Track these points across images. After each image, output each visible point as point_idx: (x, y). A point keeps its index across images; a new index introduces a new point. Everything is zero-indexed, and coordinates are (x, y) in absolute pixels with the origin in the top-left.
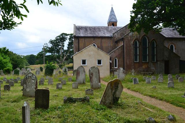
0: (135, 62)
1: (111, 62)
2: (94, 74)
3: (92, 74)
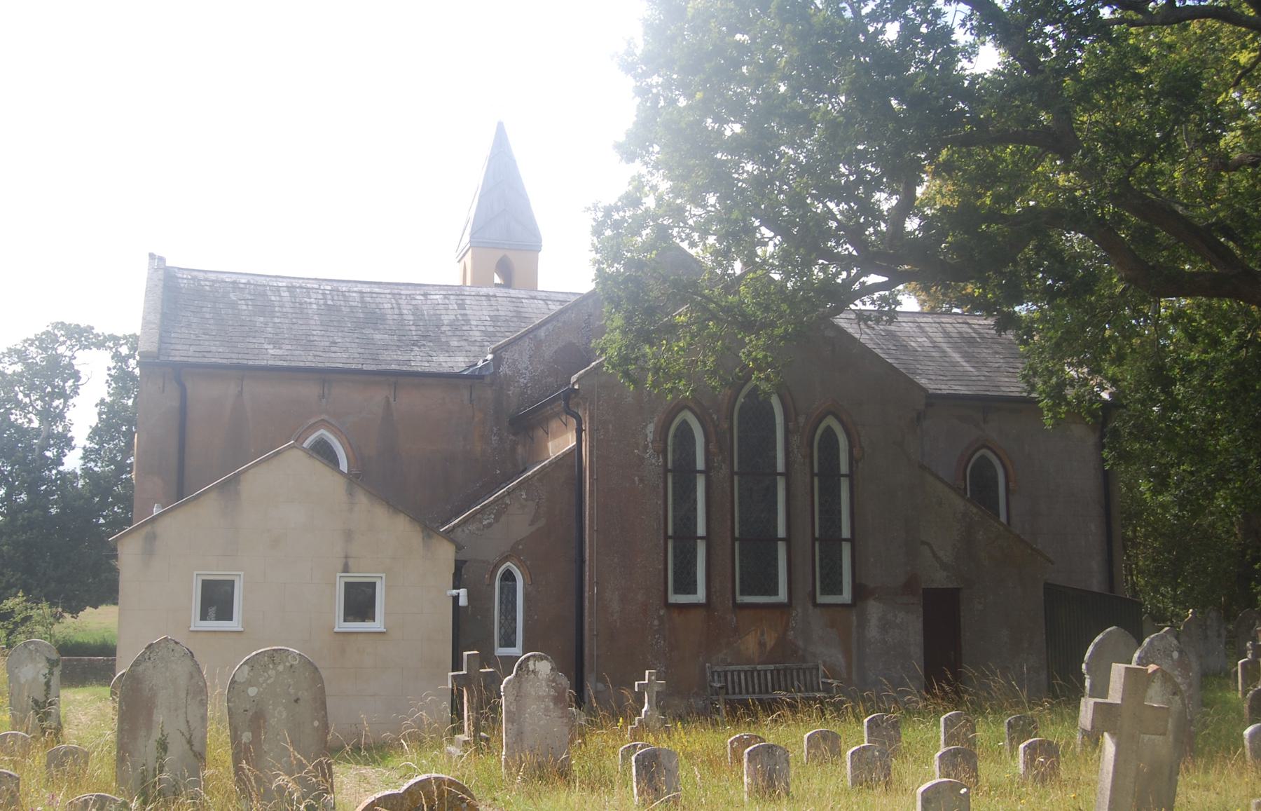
0: (674, 598)
1: (463, 601)
2: (278, 715)
3: (257, 720)
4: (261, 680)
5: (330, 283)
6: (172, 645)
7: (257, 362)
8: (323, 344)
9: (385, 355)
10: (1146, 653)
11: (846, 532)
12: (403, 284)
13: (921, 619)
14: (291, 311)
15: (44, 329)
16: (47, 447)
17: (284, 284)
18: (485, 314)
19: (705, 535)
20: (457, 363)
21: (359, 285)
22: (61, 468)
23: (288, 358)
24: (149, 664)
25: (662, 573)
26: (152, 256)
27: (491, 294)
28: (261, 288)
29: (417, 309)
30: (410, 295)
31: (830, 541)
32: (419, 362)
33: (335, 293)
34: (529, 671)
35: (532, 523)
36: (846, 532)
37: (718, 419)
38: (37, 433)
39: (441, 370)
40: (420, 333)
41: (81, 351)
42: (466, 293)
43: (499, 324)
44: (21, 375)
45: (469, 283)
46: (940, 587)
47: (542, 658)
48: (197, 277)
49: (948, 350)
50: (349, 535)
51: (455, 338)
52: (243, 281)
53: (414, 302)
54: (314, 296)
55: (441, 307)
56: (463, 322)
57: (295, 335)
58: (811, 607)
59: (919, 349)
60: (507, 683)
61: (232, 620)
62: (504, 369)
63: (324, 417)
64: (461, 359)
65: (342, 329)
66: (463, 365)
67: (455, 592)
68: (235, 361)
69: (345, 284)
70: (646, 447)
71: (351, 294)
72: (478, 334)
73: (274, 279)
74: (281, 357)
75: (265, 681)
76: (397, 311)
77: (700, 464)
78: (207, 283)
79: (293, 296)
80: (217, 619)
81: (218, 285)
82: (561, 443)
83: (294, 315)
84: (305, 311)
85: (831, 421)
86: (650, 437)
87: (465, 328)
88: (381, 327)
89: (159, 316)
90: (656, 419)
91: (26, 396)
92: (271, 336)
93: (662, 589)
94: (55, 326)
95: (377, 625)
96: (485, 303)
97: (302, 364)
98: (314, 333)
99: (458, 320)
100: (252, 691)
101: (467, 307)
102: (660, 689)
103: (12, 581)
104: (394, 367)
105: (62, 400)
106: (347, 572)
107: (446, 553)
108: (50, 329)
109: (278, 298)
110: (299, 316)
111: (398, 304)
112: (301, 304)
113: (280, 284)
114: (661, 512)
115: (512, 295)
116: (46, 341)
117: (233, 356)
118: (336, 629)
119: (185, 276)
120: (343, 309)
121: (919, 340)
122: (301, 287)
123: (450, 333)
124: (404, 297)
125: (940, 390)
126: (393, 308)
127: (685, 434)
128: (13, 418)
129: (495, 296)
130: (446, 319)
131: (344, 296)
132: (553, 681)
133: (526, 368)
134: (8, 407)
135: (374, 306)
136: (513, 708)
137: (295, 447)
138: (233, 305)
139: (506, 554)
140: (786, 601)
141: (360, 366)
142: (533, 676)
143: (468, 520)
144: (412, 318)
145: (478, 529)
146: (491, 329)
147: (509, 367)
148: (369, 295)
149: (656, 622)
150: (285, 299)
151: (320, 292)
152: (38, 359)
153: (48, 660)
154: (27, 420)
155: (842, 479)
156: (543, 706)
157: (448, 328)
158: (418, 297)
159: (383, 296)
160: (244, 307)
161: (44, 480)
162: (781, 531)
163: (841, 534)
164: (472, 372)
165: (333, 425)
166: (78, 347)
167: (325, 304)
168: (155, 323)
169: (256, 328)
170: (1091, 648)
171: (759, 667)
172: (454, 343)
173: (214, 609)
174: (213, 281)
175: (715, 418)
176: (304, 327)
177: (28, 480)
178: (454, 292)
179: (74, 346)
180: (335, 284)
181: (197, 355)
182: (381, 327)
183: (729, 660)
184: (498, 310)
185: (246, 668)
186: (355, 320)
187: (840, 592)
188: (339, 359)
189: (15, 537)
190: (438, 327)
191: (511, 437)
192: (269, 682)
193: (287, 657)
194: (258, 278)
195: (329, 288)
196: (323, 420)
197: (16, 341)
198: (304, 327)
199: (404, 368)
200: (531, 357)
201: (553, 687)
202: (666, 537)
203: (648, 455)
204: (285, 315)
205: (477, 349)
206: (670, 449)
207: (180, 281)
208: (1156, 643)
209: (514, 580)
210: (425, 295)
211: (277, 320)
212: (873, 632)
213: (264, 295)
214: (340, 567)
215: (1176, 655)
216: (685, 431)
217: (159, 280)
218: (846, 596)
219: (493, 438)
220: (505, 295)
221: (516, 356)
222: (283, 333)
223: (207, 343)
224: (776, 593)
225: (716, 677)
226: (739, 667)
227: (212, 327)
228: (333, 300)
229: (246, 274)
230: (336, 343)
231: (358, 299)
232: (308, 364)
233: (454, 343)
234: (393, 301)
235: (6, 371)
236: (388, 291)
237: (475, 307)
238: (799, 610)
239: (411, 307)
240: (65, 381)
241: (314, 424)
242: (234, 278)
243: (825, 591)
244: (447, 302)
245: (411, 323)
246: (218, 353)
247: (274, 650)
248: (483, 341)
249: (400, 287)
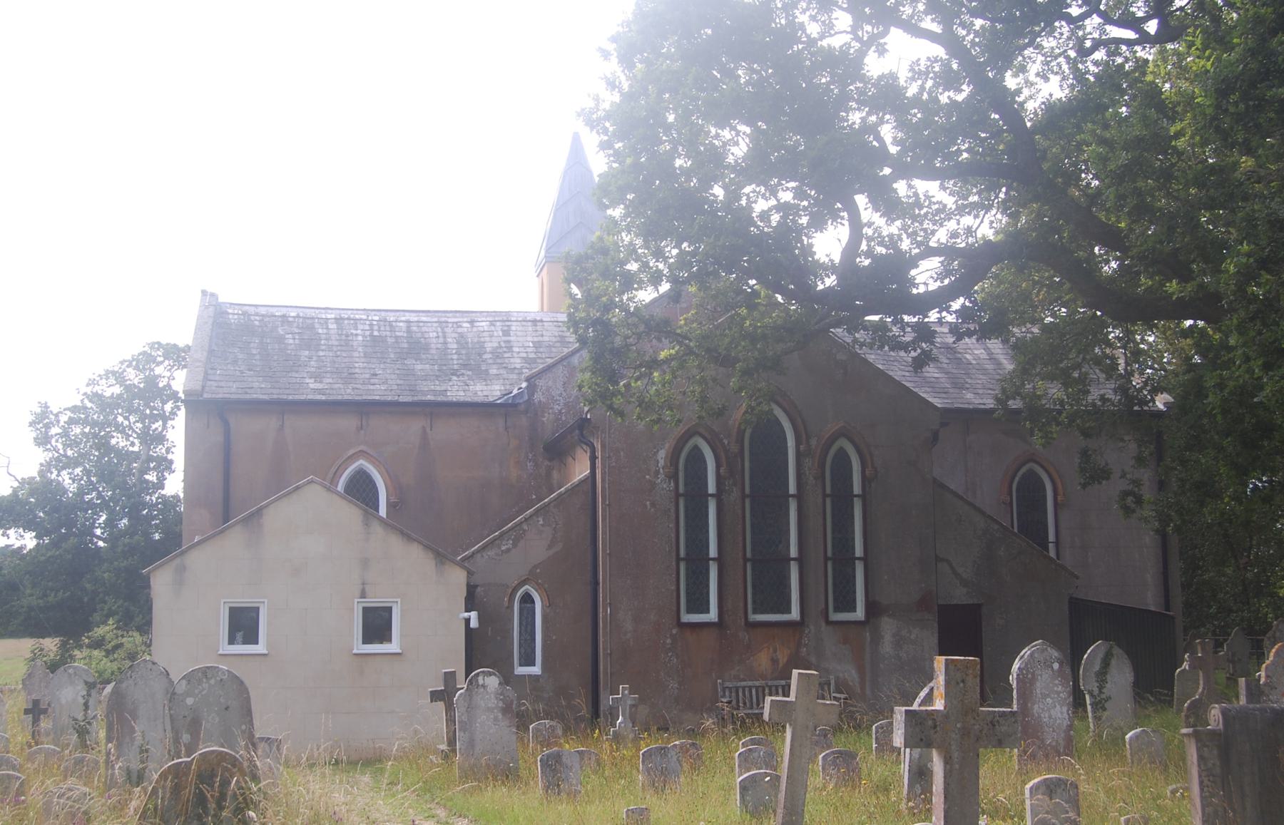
1: (474, 624)
4: (196, 691)
5: (378, 313)
6: (150, 666)
7: (297, 397)
8: (363, 376)
9: (424, 386)
10: (1026, 665)
11: (859, 552)
12: (451, 312)
13: (936, 635)
14: (336, 343)
15: (142, 350)
16: (146, 470)
17: (333, 316)
18: (529, 341)
19: (716, 556)
20: (490, 391)
21: (407, 314)
22: (163, 492)
23: (328, 392)
24: (131, 682)
25: (675, 594)
26: (204, 293)
27: (538, 319)
28: (309, 321)
29: (462, 337)
30: (457, 323)
31: (843, 559)
32: (456, 391)
33: (382, 323)
34: (478, 685)
35: (550, 547)
36: (859, 552)
37: (729, 443)
38: (136, 456)
39: (476, 399)
40: (461, 361)
41: (179, 371)
42: (513, 319)
43: (541, 350)
44: (119, 396)
46: (959, 603)
47: (490, 674)
48: (246, 313)
49: (1005, 362)
50: (365, 563)
51: (495, 366)
52: (293, 314)
53: (460, 330)
54: (361, 327)
55: (485, 334)
56: (505, 349)
57: (337, 369)
58: (823, 624)
59: (974, 362)
60: (459, 697)
61: (257, 643)
62: (538, 397)
63: (362, 447)
64: (497, 387)
65: (385, 360)
66: (498, 393)
67: (466, 615)
68: (275, 397)
69: (393, 314)
70: (657, 472)
71: (398, 324)
72: (518, 361)
73: (323, 311)
74: (320, 391)
75: (200, 692)
76: (441, 340)
78: (257, 318)
79: (340, 328)
80: (245, 643)
81: (267, 319)
82: (580, 470)
83: (339, 348)
84: (351, 343)
86: (662, 463)
87: (506, 355)
88: (424, 356)
89: (205, 354)
90: (667, 445)
91: (127, 418)
92: (313, 370)
93: (675, 609)
94: (152, 346)
95: (393, 647)
96: (530, 329)
97: (340, 397)
98: (357, 365)
99: (501, 347)
100: (190, 701)
101: (512, 333)
102: (633, 702)
103: (113, 608)
104: (430, 397)
105: (160, 423)
106: (365, 598)
107: (458, 578)
108: (146, 349)
109: (325, 331)
110: (343, 348)
111: (444, 333)
112: (347, 336)
113: (329, 316)
114: (673, 535)
115: (559, 320)
117: (275, 391)
118: (355, 651)
119: (236, 312)
120: (389, 339)
121: (976, 352)
122: (349, 319)
123: (490, 361)
124: (450, 325)
125: (984, 404)
126: (438, 337)
127: (696, 459)
128: (113, 441)
129: (542, 321)
130: (489, 346)
131: (391, 326)
132: (501, 694)
133: (560, 395)
134: (107, 430)
135: (419, 335)
136: (464, 718)
137: (312, 481)
138: (281, 339)
139: (523, 578)
140: (799, 618)
141: (396, 398)
142: (482, 690)
143: (487, 546)
144: (455, 346)
145: (497, 555)
146: (532, 356)
147: (543, 394)
148: (415, 324)
149: (669, 641)
150: (332, 332)
151: (368, 322)
152: (136, 382)
153: (86, 683)
154: (129, 443)
156: (492, 716)
157: (490, 356)
158: (465, 325)
159: (429, 324)
160: (291, 341)
161: (144, 505)
163: (854, 553)
164: (506, 400)
165: (372, 456)
166: (176, 367)
167: (371, 335)
168: (200, 361)
169: (300, 363)
171: (770, 683)
172: (493, 371)
173: (241, 633)
174: (263, 315)
175: (726, 443)
176: (346, 360)
177: (129, 505)
178: (500, 319)
179: (173, 367)
180: (383, 314)
181: (240, 391)
182: (424, 356)
183: (742, 677)
184: (542, 336)
185: (184, 682)
186: (398, 350)
187: (707, 611)
188: (378, 391)
189: (116, 563)
190: (480, 355)
191: (547, 463)
192: (203, 693)
193: (217, 672)
194: (308, 310)
195: (377, 318)
197: (112, 363)
198: (346, 360)
199: (440, 399)
200: (565, 384)
201: (501, 700)
202: (678, 559)
203: (659, 480)
204: (330, 348)
205: (515, 376)
206: (681, 475)
207: (231, 316)
208: (1036, 655)
209: (533, 602)
210: (472, 322)
211: (321, 353)
212: (887, 647)
213: (312, 327)
214: (358, 593)
215: (1056, 666)
216: (697, 457)
217: (209, 317)
218: (860, 614)
219: (528, 464)
220: (552, 320)
221: (550, 383)
222: (325, 366)
223: (250, 379)
224: (789, 611)
225: (727, 693)
226: (750, 683)
227: (258, 363)
228: (379, 331)
229: (296, 307)
230: (376, 375)
231: (404, 329)
232: (346, 397)
233: (493, 371)
234: (439, 329)
235: (104, 394)
236: (436, 320)
237: (519, 333)
238: (812, 627)
239: (456, 335)
240: (164, 403)
241: (354, 454)
242: (284, 311)
243: (838, 609)
244: (493, 328)
245: (454, 351)
246: (260, 389)
247: (207, 667)
248: (522, 368)
249: (448, 315)
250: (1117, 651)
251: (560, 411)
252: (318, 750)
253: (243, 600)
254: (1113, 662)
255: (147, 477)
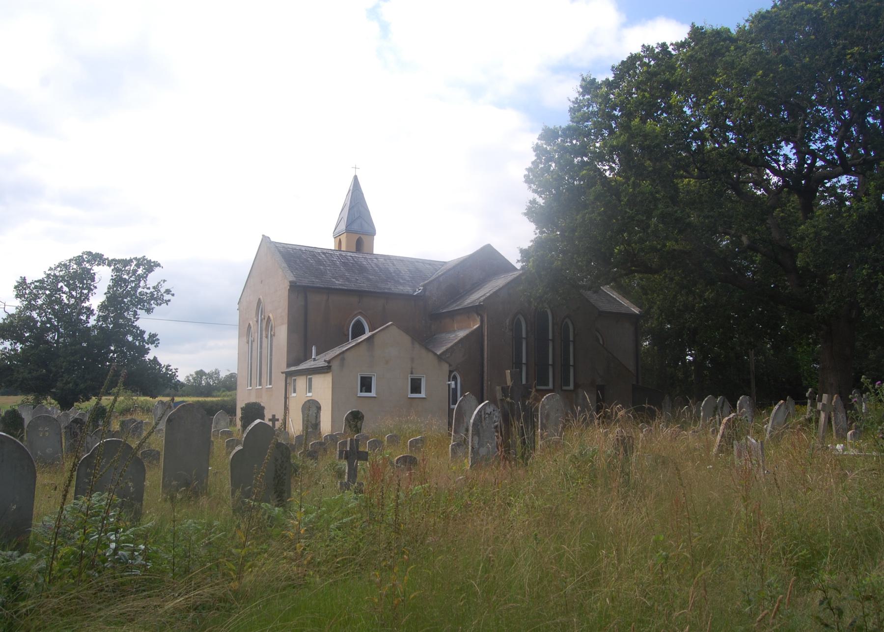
11: (572, 363)
26: (263, 236)
31: (565, 366)
36: (572, 363)
45: (344, 248)
50: (412, 360)
61: (420, 393)
62: (427, 293)
63: (360, 311)
77: (524, 335)
80: (366, 392)
85: (567, 320)
86: (508, 324)
104: (386, 291)
116: (79, 260)
127: (519, 324)
155: (571, 343)
162: (550, 362)
170: (704, 402)
196: (360, 312)
218: (571, 387)
246: (318, 283)
250: (726, 400)
251: (435, 301)
252: (789, 413)
253: (366, 374)
254: (725, 404)
255: (82, 317)
